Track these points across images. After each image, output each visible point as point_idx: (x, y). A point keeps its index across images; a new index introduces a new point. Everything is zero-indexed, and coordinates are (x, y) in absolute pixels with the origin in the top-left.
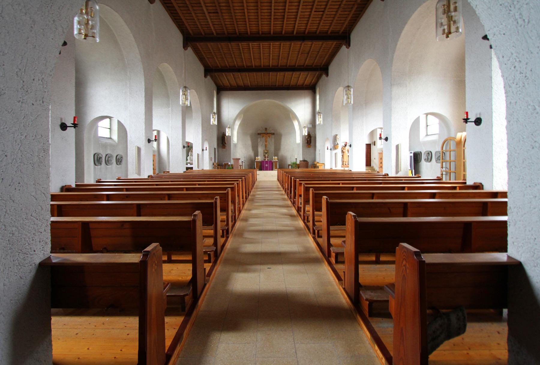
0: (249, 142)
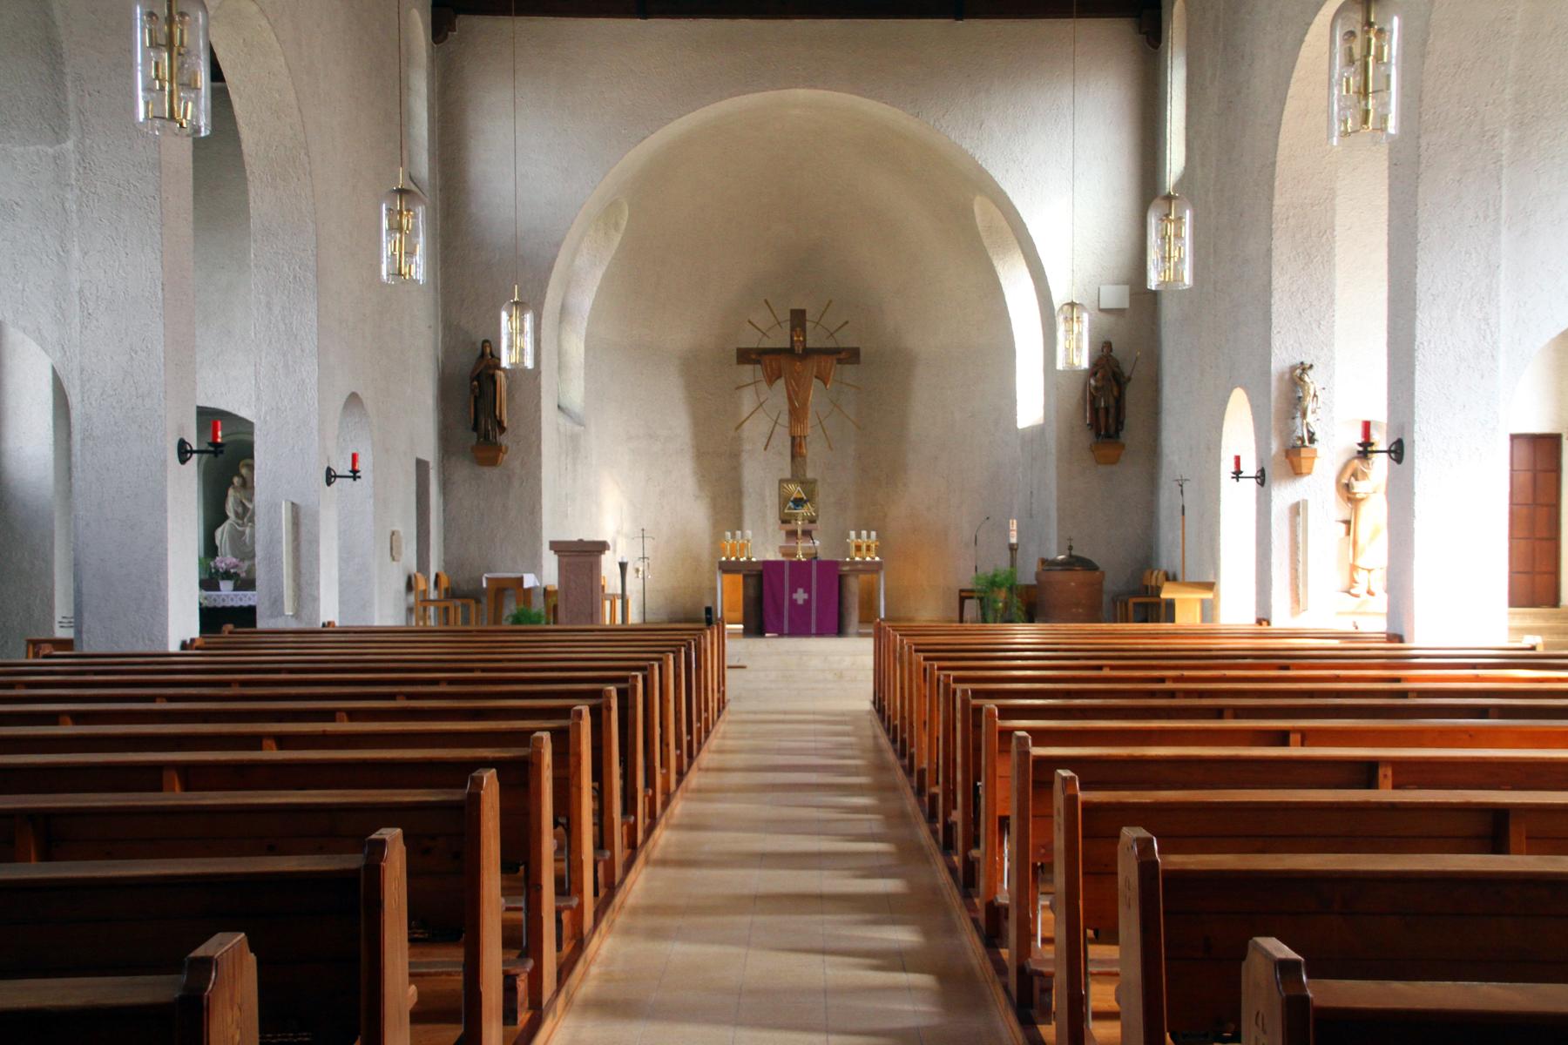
0: (679, 425)
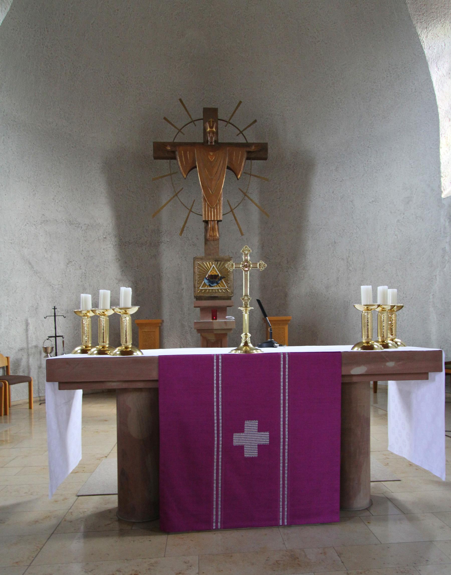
0: (103, 216)
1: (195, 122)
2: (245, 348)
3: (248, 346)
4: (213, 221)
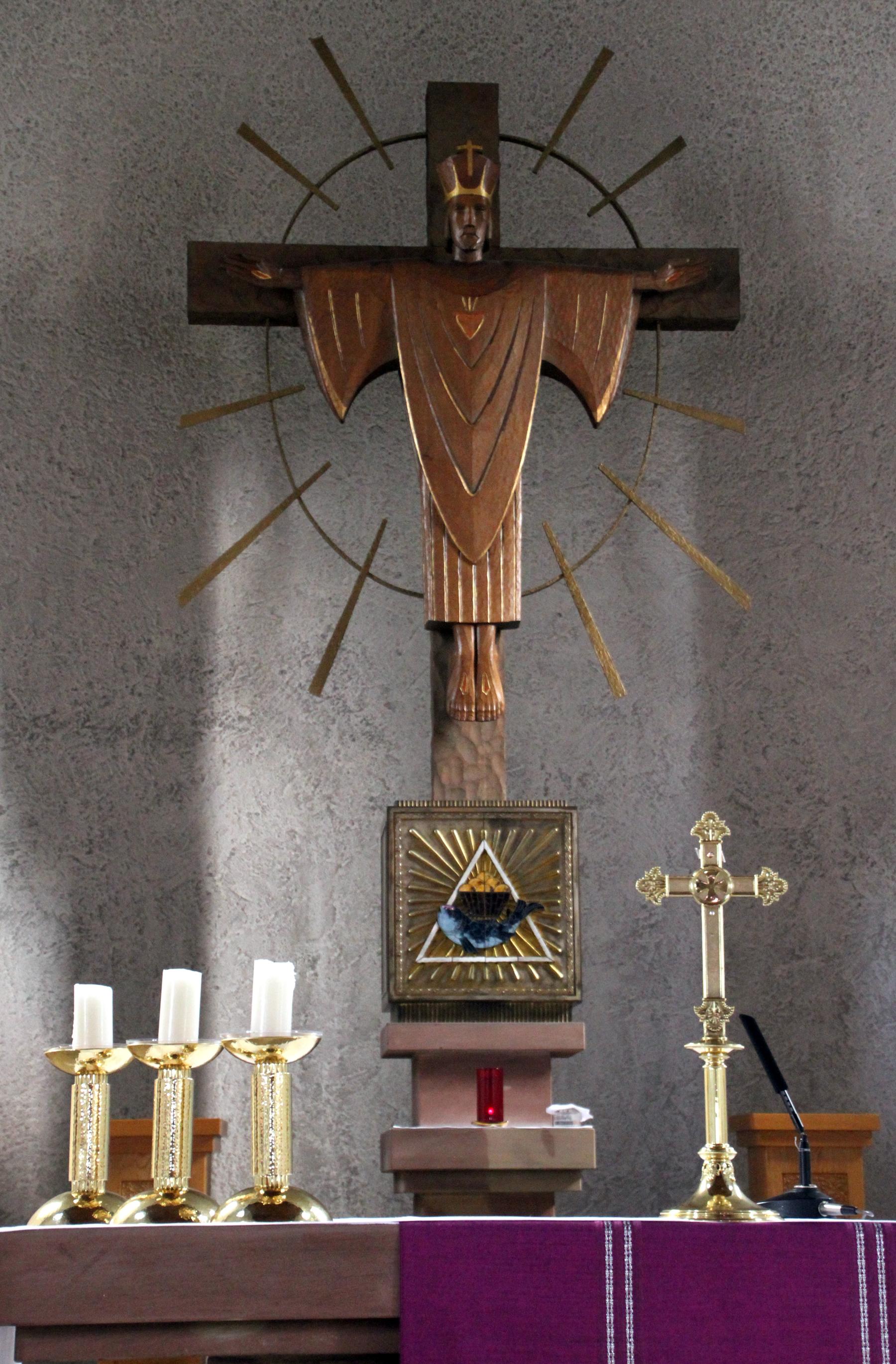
1: (389, 149)
2: (715, 1198)
3: (727, 1193)
4: (475, 625)
